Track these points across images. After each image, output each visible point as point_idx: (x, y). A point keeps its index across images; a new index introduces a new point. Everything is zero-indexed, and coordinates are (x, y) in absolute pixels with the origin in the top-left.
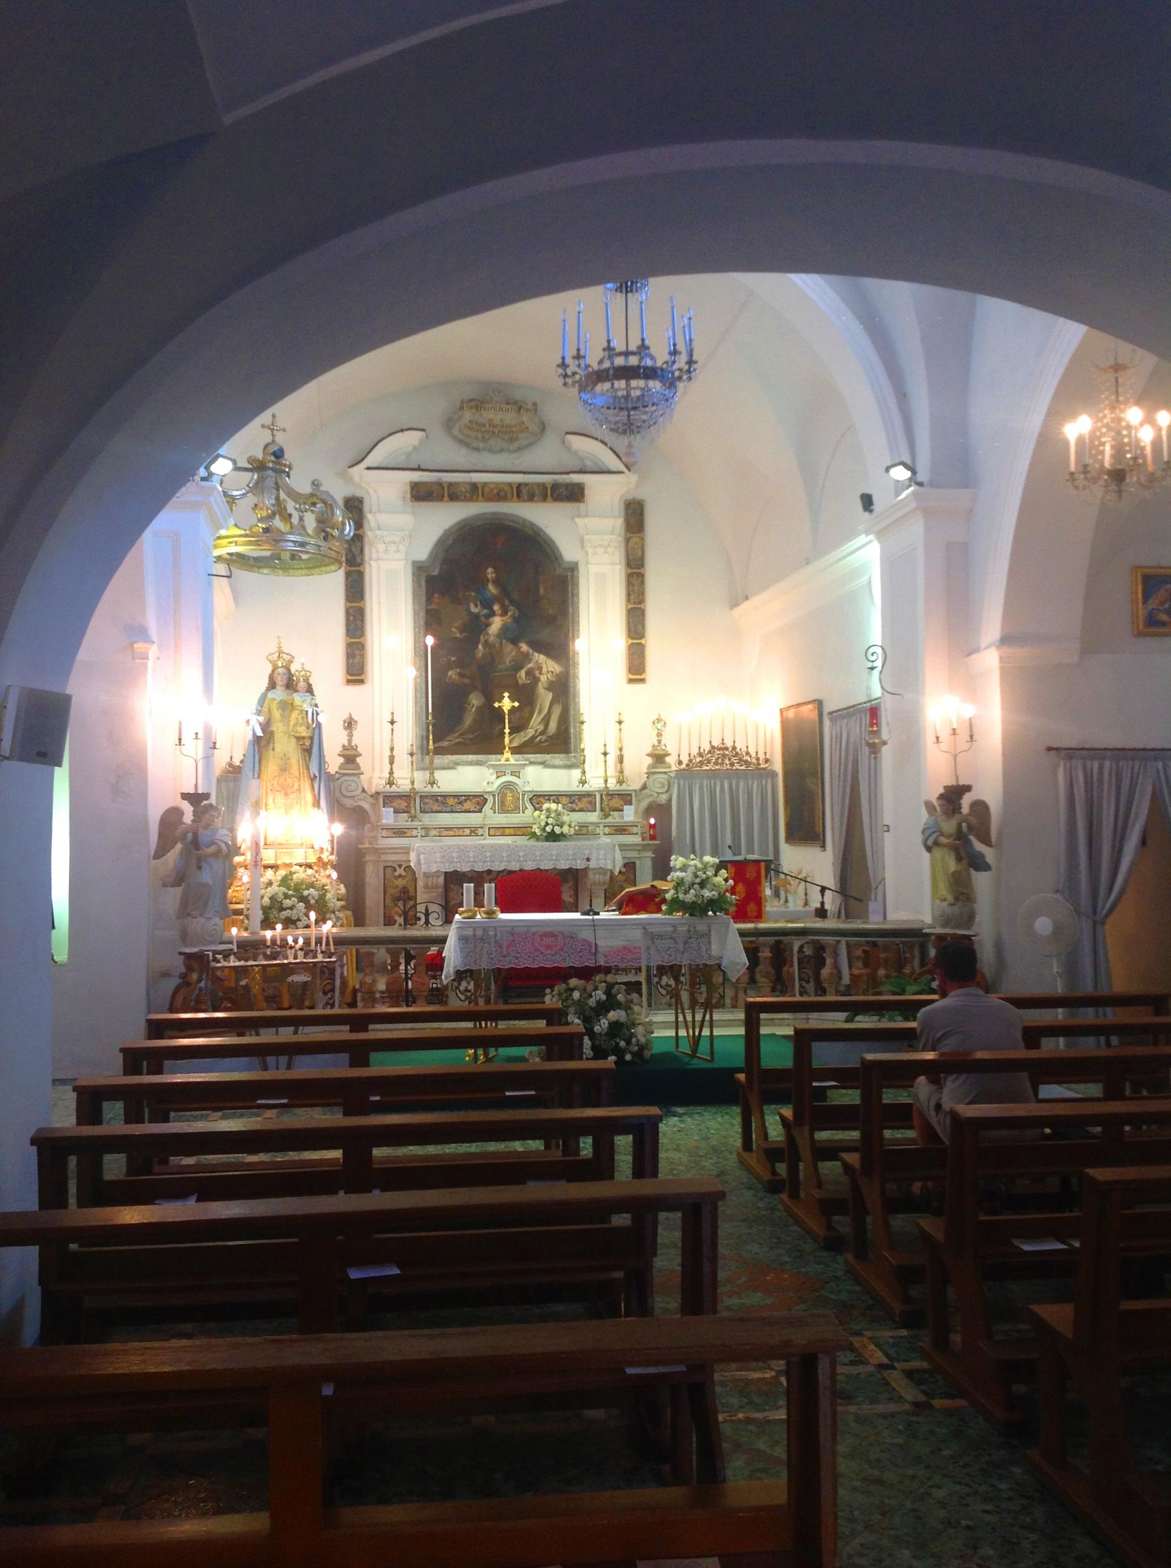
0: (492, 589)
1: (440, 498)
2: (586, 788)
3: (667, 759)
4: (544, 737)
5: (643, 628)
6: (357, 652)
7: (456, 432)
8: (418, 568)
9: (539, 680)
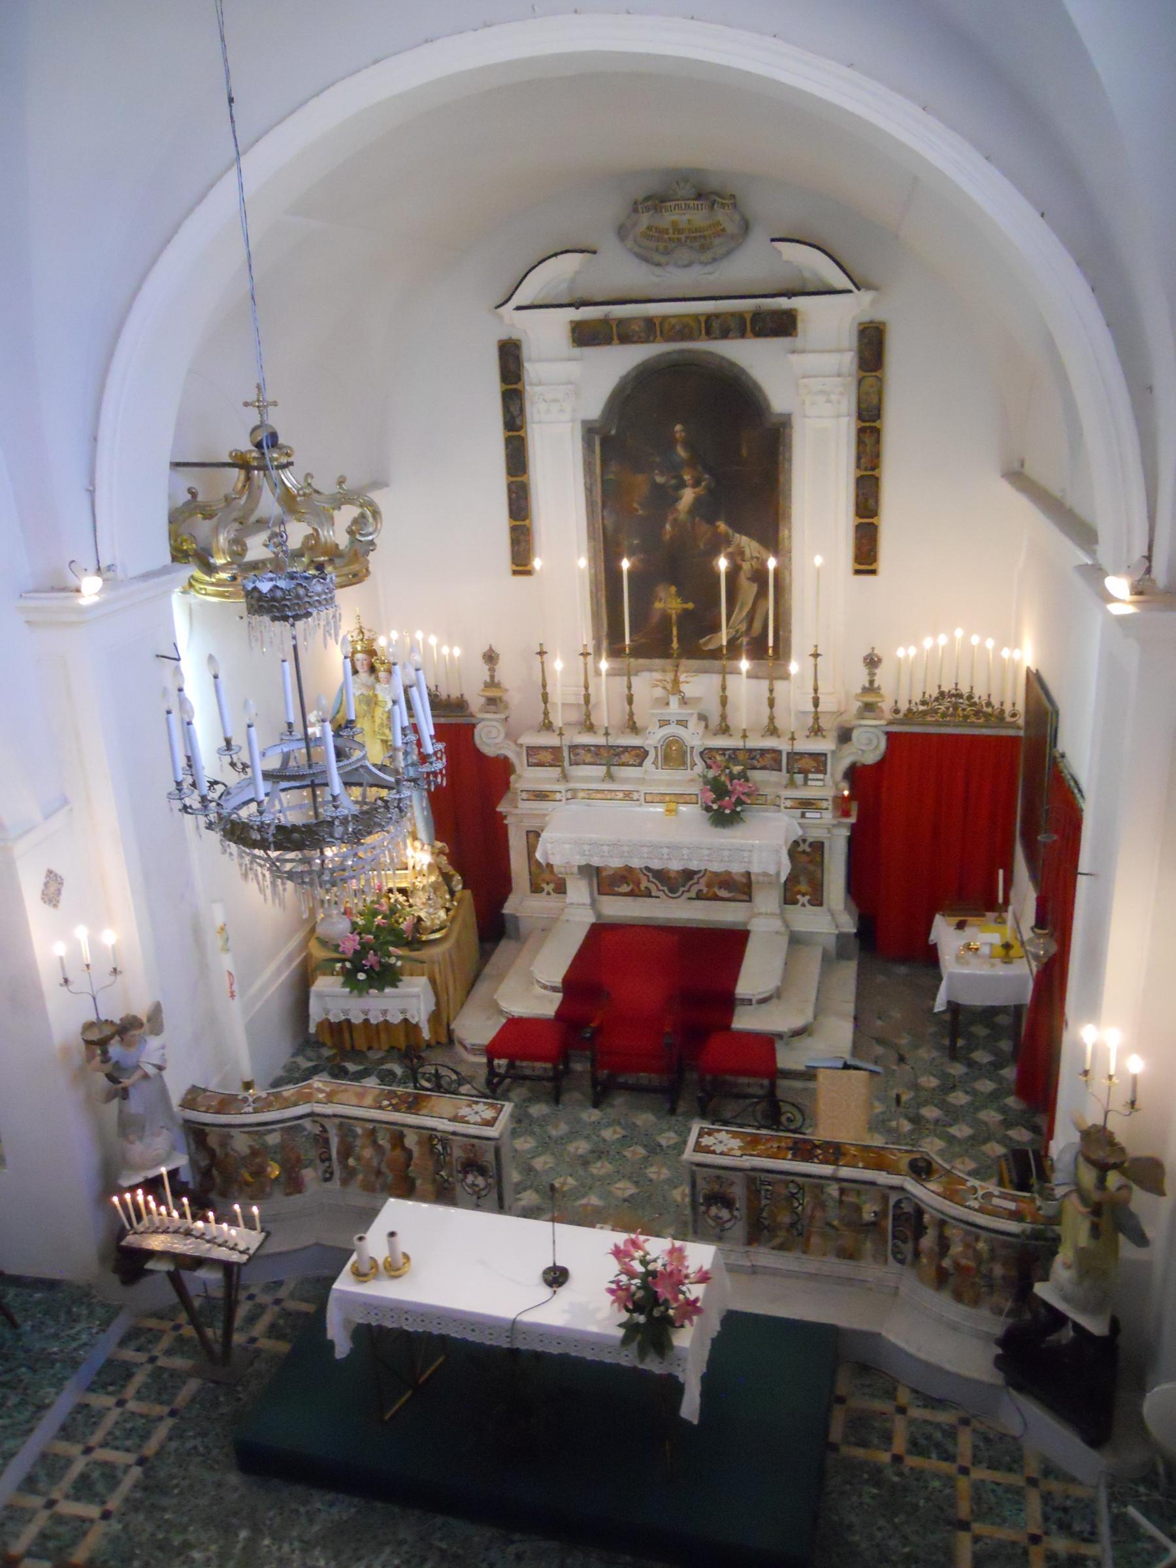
0: (681, 452)
1: (608, 341)
5: (877, 502)
6: (522, 537)
8: (590, 431)
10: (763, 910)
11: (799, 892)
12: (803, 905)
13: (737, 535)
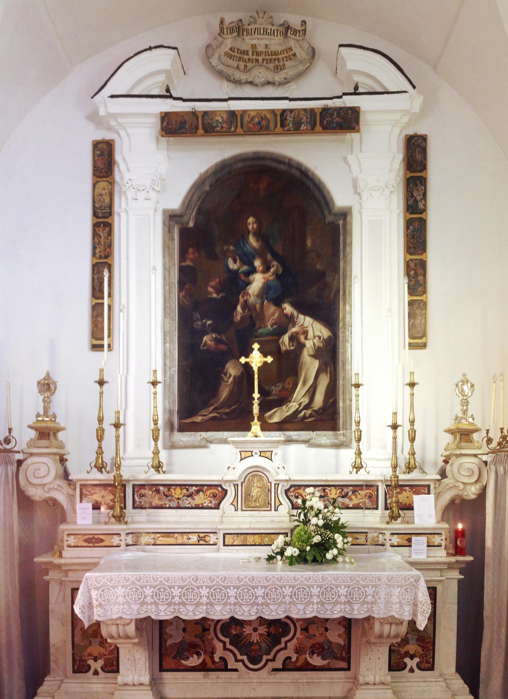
0: (253, 241)
2: (362, 476)
3: (475, 436)
4: (309, 412)
7: (215, 62)
9: (304, 346)
10: (370, 679)
11: (407, 654)
12: (412, 670)
13: (301, 317)
